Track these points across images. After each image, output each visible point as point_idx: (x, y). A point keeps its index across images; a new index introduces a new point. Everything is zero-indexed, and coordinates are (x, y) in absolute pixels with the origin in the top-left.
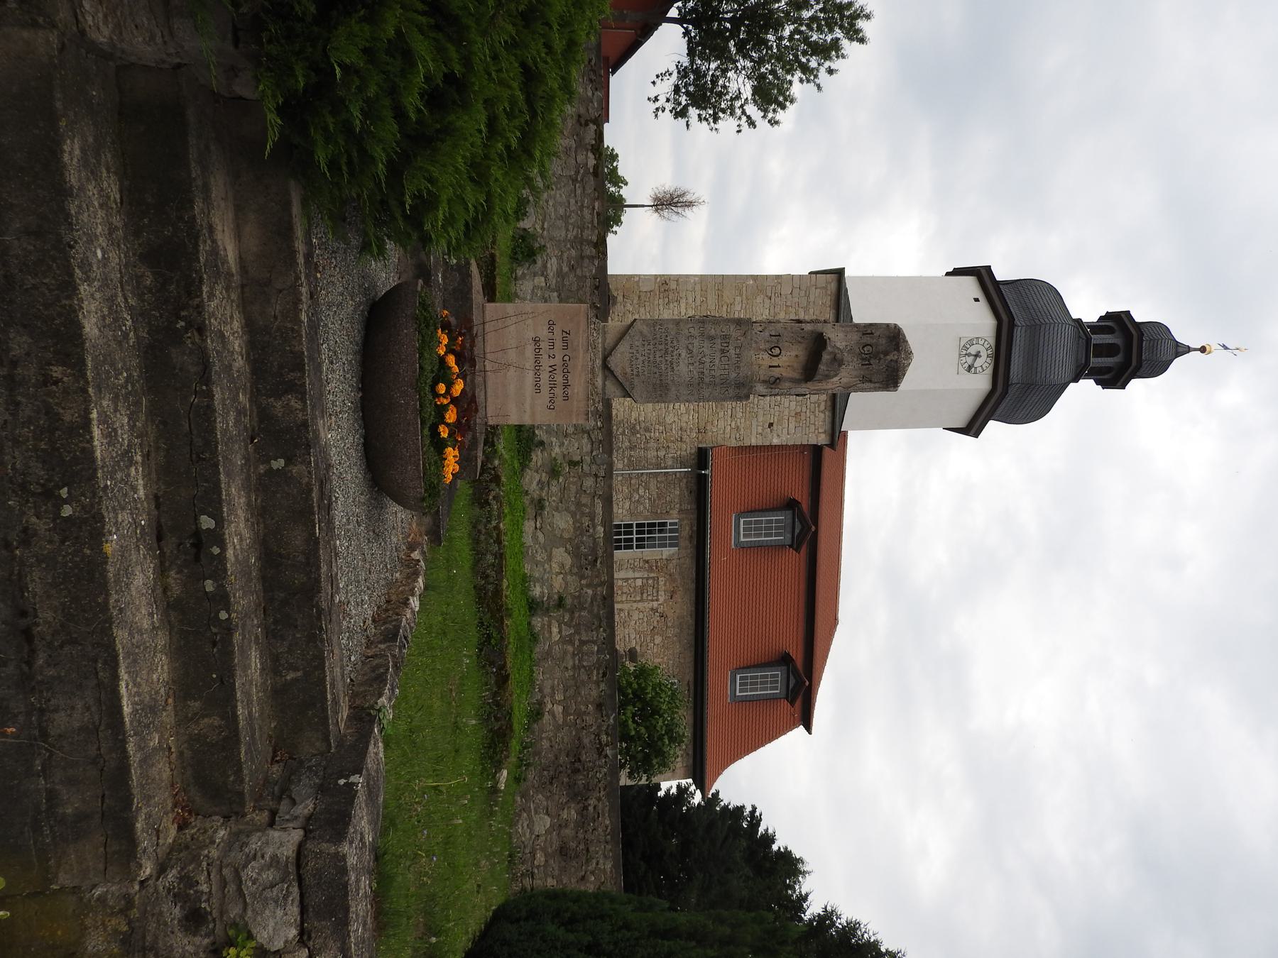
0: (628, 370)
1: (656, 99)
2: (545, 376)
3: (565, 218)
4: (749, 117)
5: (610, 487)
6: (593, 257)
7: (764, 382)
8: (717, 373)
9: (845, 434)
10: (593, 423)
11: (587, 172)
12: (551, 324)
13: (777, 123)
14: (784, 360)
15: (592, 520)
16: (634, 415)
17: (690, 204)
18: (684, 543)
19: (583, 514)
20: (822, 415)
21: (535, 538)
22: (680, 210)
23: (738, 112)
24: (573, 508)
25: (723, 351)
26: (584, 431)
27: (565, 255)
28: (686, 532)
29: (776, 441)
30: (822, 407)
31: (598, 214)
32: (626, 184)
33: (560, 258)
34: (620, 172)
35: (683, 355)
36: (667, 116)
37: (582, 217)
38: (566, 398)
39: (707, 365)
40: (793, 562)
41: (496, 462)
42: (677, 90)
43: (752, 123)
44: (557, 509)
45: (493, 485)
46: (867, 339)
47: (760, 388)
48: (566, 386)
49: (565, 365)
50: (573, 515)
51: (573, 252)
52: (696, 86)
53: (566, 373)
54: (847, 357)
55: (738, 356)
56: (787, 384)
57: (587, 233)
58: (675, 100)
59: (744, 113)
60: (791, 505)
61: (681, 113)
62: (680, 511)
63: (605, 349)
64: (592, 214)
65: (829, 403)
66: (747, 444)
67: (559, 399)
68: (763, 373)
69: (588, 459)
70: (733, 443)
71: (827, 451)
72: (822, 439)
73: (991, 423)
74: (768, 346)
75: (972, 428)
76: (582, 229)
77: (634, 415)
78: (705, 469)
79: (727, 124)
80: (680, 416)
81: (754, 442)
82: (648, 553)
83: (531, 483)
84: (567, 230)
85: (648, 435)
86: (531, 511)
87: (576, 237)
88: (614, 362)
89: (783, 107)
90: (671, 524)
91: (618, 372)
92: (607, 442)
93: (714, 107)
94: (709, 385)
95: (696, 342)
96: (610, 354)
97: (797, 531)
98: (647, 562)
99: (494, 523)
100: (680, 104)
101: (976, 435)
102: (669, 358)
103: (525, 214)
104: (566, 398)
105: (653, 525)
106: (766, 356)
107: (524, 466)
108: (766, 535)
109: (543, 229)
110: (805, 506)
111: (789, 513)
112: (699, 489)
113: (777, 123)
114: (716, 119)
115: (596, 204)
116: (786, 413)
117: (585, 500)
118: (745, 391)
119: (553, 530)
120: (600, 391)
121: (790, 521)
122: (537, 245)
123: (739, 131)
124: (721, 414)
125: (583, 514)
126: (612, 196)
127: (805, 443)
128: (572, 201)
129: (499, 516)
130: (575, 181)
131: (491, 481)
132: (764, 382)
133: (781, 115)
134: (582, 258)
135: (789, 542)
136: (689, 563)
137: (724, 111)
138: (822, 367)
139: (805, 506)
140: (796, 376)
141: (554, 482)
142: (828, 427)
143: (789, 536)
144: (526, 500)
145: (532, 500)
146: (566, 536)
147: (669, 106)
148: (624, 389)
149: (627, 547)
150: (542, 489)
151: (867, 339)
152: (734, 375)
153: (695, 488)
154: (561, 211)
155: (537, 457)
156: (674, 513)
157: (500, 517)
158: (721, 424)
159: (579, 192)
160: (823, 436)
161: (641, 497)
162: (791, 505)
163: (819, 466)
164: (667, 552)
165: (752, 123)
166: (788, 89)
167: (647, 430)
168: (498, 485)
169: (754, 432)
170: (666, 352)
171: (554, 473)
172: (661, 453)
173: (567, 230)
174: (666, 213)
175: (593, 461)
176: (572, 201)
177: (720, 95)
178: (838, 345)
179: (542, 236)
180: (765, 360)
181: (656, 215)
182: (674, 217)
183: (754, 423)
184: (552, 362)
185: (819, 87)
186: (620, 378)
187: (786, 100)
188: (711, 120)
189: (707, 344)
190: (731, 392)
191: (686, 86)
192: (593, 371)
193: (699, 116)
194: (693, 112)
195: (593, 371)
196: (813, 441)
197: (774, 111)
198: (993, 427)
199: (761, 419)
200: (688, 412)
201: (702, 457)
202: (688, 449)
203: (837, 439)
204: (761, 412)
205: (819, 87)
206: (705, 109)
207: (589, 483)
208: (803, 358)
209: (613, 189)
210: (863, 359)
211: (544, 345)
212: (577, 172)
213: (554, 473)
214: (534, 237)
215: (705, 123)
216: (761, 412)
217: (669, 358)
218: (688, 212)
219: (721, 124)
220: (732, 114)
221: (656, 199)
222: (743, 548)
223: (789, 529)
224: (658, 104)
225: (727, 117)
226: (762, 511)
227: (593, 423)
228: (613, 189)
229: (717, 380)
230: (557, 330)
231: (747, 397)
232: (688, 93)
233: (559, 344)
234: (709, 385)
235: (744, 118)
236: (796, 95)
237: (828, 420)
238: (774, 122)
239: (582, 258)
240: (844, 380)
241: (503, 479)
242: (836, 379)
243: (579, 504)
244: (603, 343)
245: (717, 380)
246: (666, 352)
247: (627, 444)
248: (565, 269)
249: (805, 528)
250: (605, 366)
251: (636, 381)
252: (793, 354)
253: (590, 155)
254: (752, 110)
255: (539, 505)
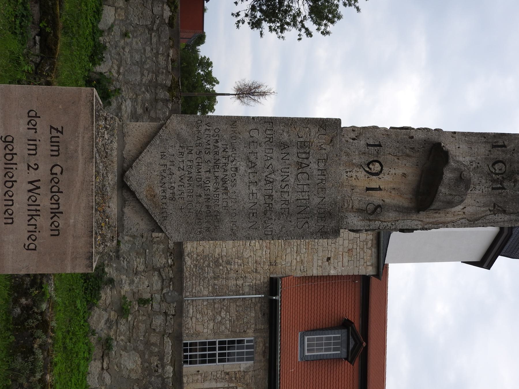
0: (158, 191)
1: (238, 15)
2: (21, 196)
3: (141, 64)
4: (307, 29)
5: (180, 325)
6: (167, 101)
7: (360, 211)
8: (293, 197)
9: (387, 265)
10: (164, 261)
11: (162, 22)
12: (32, 117)
13: (328, 33)
14: (386, 180)
15: (161, 359)
16: (218, 251)
17: (263, 94)
18: (258, 357)
19: (151, 354)
20: (369, 251)
21: (101, 379)
22: (256, 98)
23: (299, 26)
24: (141, 347)
25: (300, 165)
26: (154, 269)
27: (140, 98)
28: (260, 348)
29: (333, 272)
30: (369, 245)
31: (173, 61)
32: (218, 83)
33: (134, 101)
34: (214, 75)
35: (242, 168)
36: (246, 27)
37: (157, 63)
38: (56, 232)
39: (278, 185)
40: (348, 372)
41: (44, 306)
42: (253, 8)
43: (309, 34)
44: (125, 349)
45: (39, 332)
46: (498, 154)
47: (354, 220)
48: (55, 213)
49: (54, 179)
50: (142, 355)
51: (148, 96)
52: (268, 6)
53: (56, 192)
54: (475, 179)
55: (323, 172)
56: (392, 215)
57: (161, 78)
58: (252, 15)
59: (303, 26)
60: (346, 324)
61: (256, 24)
62: (256, 331)
63: (122, 159)
64: (166, 60)
65: (375, 242)
66: (310, 274)
67: (44, 235)
68: (358, 200)
69: (158, 296)
70: (299, 274)
71: (374, 281)
72: (370, 271)
73: (500, 257)
74: (365, 159)
75: (486, 261)
76: (157, 73)
77: (218, 251)
78: (276, 295)
79: (291, 33)
80: (255, 252)
81: (315, 273)
82: (228, 366)
83: (99, 321)
84: (143, 75)
85: (229, 267)
86: (97, 351)
87: (150, 81)
88: (137, 178)
89: (333, 22)
90: (248, 341)
91: (142, 194)
92: (177, 279)
93: (281, 21)
94: (280, 214)
95: (261, 152)
96: (130, 166)
97: (351, 346)
98: (228, 374)
99: (38, 376)
100: (256, 17)
101: (489, 269)
102: (220, 174)
103: (102, 59)
104: (56, 232)
105: (233, 342)
106: (362, 174)
107: (91, 305)
108: (326, 350)
109: (119, 73)
110: (357, 324)
111: (344, 331)
112: (271, 312)
113: (328, 33)
114: (282, 29)
115: (171, 52)
116: (341, 249)
117: (154, 339)
118: (333, 224)
119: (121, 371)
120: (114, 222)
121: (345, 338)
122: (112, 88)
123: (300, 39)
124: (289, 250)
125: (151, 354)
126: (208, 91)
127: (356, 273)
128: (148, 49)
129: (45, 367)
130: (151, 30)
131: (37, 327)
132: (360, 211)
133: (330, 27)
134: (156, 100)
135: (344, 355)
136: (263, 375)
137: (288, 24)
138: (443, 190)
139: (357, 324)
140: (404, 202)
141: (123, 321)
142: (374, 260)
143: (345, 350)
144: (93, 340)
145: (100, 339)
146: (134, 376)
147: (247, 20)
148: (151, 219)
149: (211, 361)
150: (110, 328)
151: (498, 154)
152: (316, 200)
153: (267, 311)
154: (137, 57)
155: (107, 295)
156: (250, 332)
157: (47, 368)
158: (289, 259)
159: (154, 40)
160: (370, 268)
161: (223, 318)
162: (345, 324)
163: (368, 292)
164: (244, 365)
165: (309, 34)
166: (336, 10)
167: (228, 263)
168: (46, 332)
169: (315, 265)
170: (216, 164)
171: (123, 311)
172: (240, 282)
173: (143, 75)
174: (245, 100)
175: (164, 299)
176: (148, 49)
177: (286, 12)
178: (461, 159)
179: (117, 80)
180: (361, 179)
181: (238, 101)
182: (252, 103)
183: (315, 257)
184: (33, 175)
185: (358, 9)
186: (146, 203)
187: (334, 17)
188: (279, 30)
189: (276, 154)
190: (313, 225)
191: (260, 5)
192: (101, 191)
193: (270, 27)
194: (265, 25)
195: (101, 191)
196: (363, 272)
197: (325, 25)
198: (501, 260)
199: (320, 254)
200: (261, 248)
201: (273, 285)
202: (262, 278)
203: (381, 271)
204: (321, 249)
205: (358, 9)
206: (273, 22)
207: (158, 321)
208: (413, 178)
209: (208, 86)
210: (493, 181)
211: (20, 148)
212: (153, 23)
213: (123, 311)
214: (110, 81)
215: (274, 33)
216: (321, 249)
217: (220, 174)
218: (262, 99)
219: (286, 33)
220: (295, 25)
221: (239, 89)
222: (307, 360)
223: (345, 345)
224: (239, 18)
225: (290, 28)
226: (320, 329)
227: (164, 261)
228: (208, 86)
229: (292, 207)
230: (43, 126)
231: (336, 233)
232: (261, 10)
233: (44, 147)
234: (280, 214)
235: (303, 30)
236: (342, 13)
237: (374, 255)
238: (325, 33)
239: (156, 100)
240: (470, 210)
241: (53, 324)
242: (459, 207)
243: (148, 344)
244: (122, 146)
245: (292, 207)
246: (216, 164)
247: (212, 274)
248: (140, 111)
249: (358, 344)
250: (123, 185)
251: (170, 208)
252: (400, 171)
253: (166, 7)
254: (309, 24)
255: (107, 345)
